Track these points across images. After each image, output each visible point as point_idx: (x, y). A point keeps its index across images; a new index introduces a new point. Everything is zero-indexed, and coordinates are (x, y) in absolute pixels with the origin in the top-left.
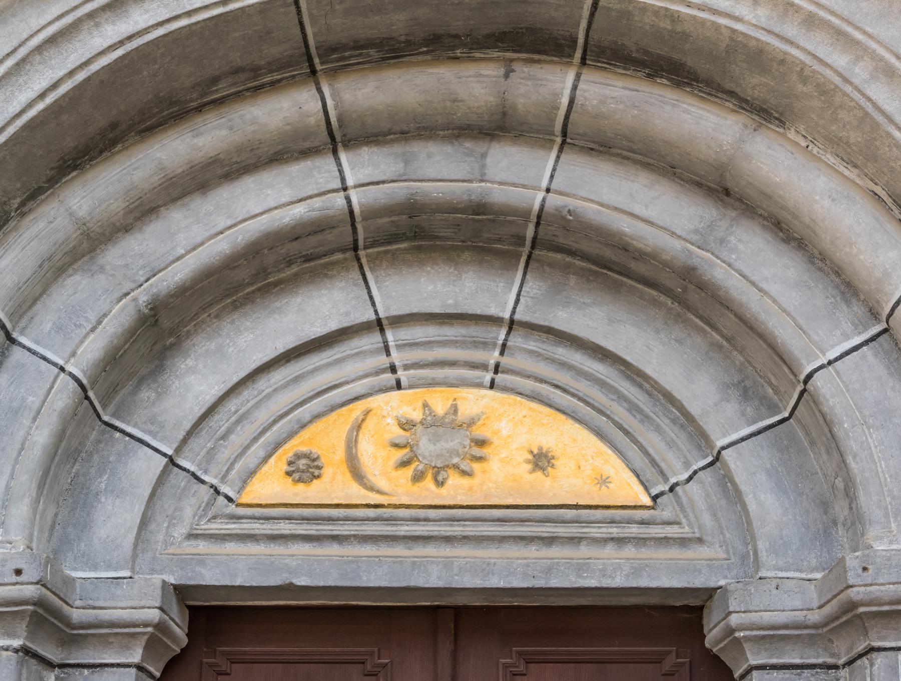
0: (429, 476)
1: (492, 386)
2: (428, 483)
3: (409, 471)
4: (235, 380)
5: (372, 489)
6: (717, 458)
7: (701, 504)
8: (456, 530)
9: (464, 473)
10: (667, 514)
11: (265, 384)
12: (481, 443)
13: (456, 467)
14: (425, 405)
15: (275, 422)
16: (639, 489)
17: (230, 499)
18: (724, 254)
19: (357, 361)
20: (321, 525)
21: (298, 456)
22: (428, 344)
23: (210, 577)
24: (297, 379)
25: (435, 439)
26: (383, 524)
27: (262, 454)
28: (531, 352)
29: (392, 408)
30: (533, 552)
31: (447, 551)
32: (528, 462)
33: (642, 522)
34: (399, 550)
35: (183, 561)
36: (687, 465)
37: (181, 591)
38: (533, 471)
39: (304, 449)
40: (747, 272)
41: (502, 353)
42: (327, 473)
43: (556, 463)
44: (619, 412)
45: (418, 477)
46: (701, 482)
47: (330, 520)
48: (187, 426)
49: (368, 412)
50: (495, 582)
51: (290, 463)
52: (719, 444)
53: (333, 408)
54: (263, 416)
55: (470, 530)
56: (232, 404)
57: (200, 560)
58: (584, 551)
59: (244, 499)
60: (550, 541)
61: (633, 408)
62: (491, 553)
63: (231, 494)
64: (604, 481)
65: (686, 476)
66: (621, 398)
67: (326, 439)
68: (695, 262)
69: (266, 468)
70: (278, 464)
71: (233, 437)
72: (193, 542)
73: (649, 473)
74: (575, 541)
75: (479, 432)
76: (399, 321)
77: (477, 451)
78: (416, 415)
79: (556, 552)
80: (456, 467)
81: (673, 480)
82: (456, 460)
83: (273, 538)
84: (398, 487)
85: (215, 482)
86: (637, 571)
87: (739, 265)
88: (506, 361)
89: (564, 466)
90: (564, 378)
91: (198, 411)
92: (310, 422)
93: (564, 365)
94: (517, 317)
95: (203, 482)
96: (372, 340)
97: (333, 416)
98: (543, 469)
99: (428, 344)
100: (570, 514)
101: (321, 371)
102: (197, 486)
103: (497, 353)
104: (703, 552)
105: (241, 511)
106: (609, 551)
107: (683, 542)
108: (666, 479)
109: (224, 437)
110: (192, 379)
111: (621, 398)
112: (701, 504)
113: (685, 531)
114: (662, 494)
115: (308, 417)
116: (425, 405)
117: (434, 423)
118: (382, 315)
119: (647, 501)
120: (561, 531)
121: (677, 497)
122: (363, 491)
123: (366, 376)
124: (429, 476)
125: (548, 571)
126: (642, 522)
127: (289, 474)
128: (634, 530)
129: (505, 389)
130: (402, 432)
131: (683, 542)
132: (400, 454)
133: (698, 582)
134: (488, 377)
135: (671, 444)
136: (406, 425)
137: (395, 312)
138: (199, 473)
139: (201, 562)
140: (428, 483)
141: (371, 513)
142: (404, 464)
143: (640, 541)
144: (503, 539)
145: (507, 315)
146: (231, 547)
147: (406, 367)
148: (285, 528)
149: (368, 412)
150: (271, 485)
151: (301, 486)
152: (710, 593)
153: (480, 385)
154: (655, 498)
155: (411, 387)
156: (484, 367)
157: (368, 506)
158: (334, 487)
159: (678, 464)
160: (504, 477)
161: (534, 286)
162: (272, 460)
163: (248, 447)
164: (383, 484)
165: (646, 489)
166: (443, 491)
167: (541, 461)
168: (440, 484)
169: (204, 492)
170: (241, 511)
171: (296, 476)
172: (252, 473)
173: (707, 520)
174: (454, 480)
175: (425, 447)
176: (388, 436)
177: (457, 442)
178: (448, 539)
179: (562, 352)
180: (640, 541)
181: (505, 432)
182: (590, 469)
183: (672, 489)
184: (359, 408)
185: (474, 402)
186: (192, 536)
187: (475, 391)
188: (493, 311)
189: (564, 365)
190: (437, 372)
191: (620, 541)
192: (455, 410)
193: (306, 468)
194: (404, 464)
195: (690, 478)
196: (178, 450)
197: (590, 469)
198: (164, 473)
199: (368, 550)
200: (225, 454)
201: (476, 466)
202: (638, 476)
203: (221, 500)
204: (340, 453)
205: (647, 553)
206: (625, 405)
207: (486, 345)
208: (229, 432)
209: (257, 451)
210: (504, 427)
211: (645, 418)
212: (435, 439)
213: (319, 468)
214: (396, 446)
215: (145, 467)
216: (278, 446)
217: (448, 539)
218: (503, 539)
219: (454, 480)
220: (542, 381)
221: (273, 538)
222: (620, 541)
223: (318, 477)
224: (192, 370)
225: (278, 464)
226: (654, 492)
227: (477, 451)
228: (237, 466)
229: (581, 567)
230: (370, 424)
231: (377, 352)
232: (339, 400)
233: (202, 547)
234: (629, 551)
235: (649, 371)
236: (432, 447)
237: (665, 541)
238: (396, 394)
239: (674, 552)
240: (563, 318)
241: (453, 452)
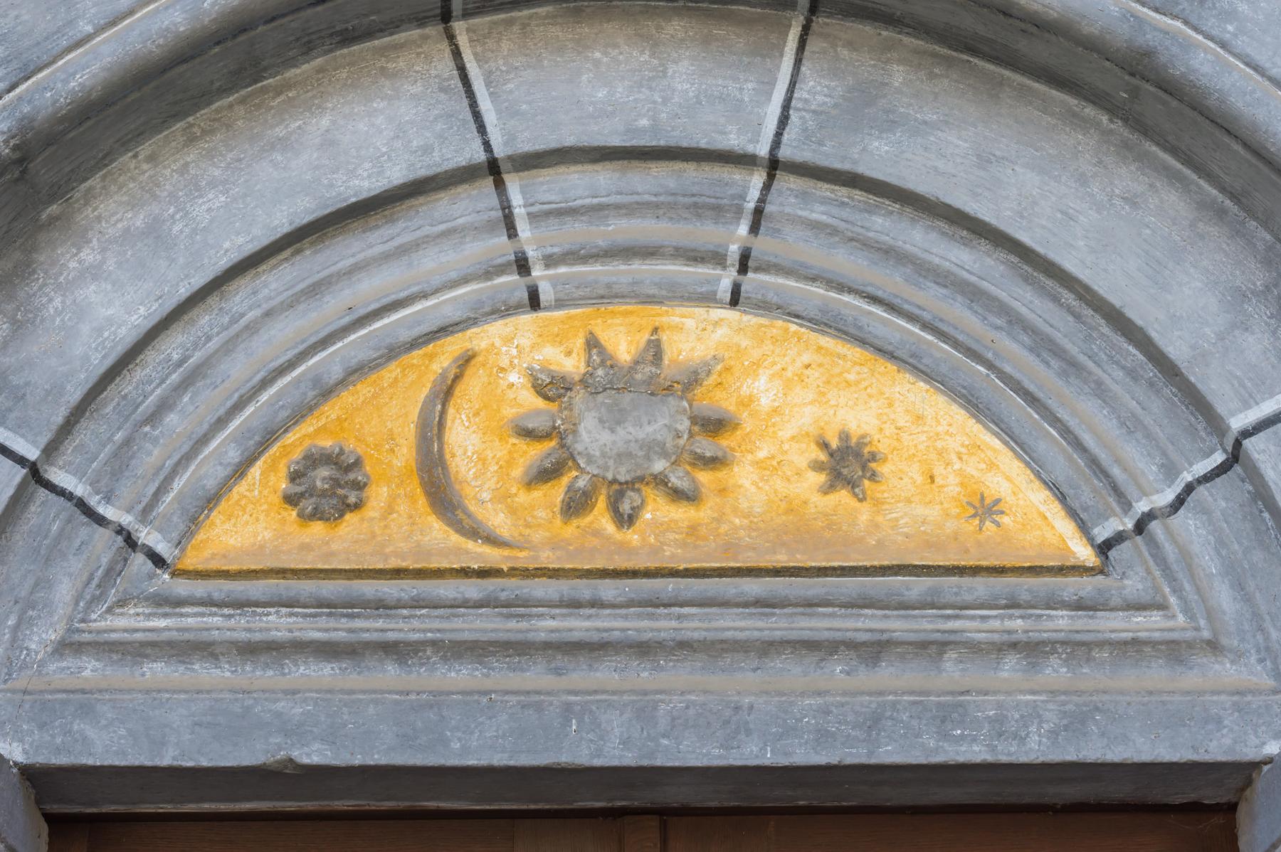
0: (602, 503)
1: (735, 300)
2: (600, 517)
3: (557, 492)
4: (184, 292)
5: (475, 532)
6: (1236, 456)
7: (1208, 563)
8: (663, 626)
9: (678, 495)
10: (1134, 585)
11: (243, 299)
12: (715, 425)
13: (660, 481)
14: (592, 343)
15: (265, 383)
16: (1065, 527)
17: (158, 560)
18: (1210, 24)
19: (444, 250)
20: (359, 617)
21: (314, 460)
22: (597, 211)
23: (104, 744)
24: (315, 290)
25: (614, 419)
26: (499, 611)
27: (234, 455)
28: (816, 226)
29: (518, 351)
30: (837, 671)
31: (642, 675)
32: (817, 466)
33: (1079, 606)
34: (535, 676)
35: (44, 707)
36: (1170, 472)
37: (736, 426)
38: (829, 488)
39: (327, 443)
40: (1262, 58)
41: (755, 229)
42: (378, 496)
43: (884, 469)
44: (1013, 352)
45: (576, 505)
46: (1205, 511)
47: (381, 606)
48: (74, 395)
49: (466, 360)
50: (754, 752)
51: (294, 477)
52: (1237, 423)
53: (393, 352)
54: (238, 370)
55: (695, 625)
56: (173, 345)
57: (84, 702)
58: (952, 671)
59: (192, 561)
60: (874, 650)
61: (1044, 345)
62: (743, 682)
63: (162, 548)
64: (986, 509)
65: (1169, 496)
66: (1015, 322)
67: (379, 421)
68: (1149, 39)
69: (241, 488)
70: (267, 480)
71: (172, 419)
72: (69, 662)
73: (1088, 493)
74: (931, 649)
75: (713, 398)
76: (531, 162)
77: (705, 446)
78: (572, 364)
79: (889, 676)
80: (660, 481)
81: (1142, 507)
82: (659, 466)
83: (251, 650)
84: (513, 511)
85: (126, 519)
86: (1076, 723)
87: (1241, 43)
88: (763, 246)
89: (898, 475)
90: (891, 281)
91: (99, 363)
92: (343, 383)
93: (890, 254)
94: (785, 153)
95: (101, 521)
96: (476, 201)
97: (392, 371)
98: (852, 484)
99: (597, 211)
100: (918, 586)
101: (367, 269)
102: (86, 530)
103: (743, 229)
104: (1226, 672)
105: (183, 588)
106: (1010, 669)
107: (1174, 651)
108: (1127, 506)
109: (154, 418)
110: (90, 292)
111: (1015, 322)
112: (1208, 563)
113: (1170, 623)
114: (1119, 538)
115: (336, 372)
116: (592, 343)
117: (610, 382)
118: (499, 151)
119: (1084, 553)
120: (897, 625)
121: (1153, 543)
122: (455, 538)
123: (465, 280)
124: (602, 503)
125: (874, 722)
126: (1079, 606)
127: (291, 500)
128: (1062, 621)
129: (765, 307)
130: (540, 403)
131: (1174, 651)
132: (535, 452)
133: (1217, 748)
134: (726, 280)
135: (1132, 426)
136: (552, 387)
137: (526, 145)
138: (93, 501)
139: (86, 710)
140: (600, 517)
141: (472, 589)
142: (545, 474)
143: (1078, 649)
144: (768, 648)
145: (763, 150)
146: (156, 671)
147: (550, 261)
148: (278, 625)
149: (466, 360)
150: (251, 526)
151: (318, 528)
152: (1244, 773)
153: (708, 299)
154: (1104, 548)
155: (560, 304)
156: (718, 258)
157: (465, 573)
158: (391, 523)
159: (1149, 470)
160: (765, 491)
161: (817, 88)
162: (256, 471)
163: (204, 440)
164: (498, 521)
165: (1084, 528)
166: (632, 536)
167: (847, 463)
168: (626, 520)
169: (103, 544)
170: (183, 588)
171: (308, 505)
172: (212, 500)
173: (1224, 598)
174: (657, 509)
175: (593, 436)
176: (509, 412)
177: (662, 423)
178: (644, 649)
179: (885, 224)
180: (1078, 649)
181: (765, 402)
182: (954, 475)
183: (1140, 527)
184: (446, 353)
185: (697, 334)
186: (68, 646)
187: (700, 312)
188: (733, 141)
189: (890, 254)
190: (620, 266)
191: (1033, 650)
192: (655, 351)
193: (329, 487)
194: (545, 474)
195: (1179, 502)
196: (51, 450)
197: (954, 475)
198: (22, 487)
199: (461, 676)
200: (152, 456)
201: (704, 477)
202: (1062, 498)
203: (139, 561)
204: (405, 454)
205: (1092, 677)
206: (1021, 334)
207: (720, 211)
208: (164, 406)
209: (224, 448)
210: (762, 389)
211: (1072, 367)
212: (614, 419)
213: (359, 486)
214: (528, 434)
215: (43, 552)
216: (269, 437)
217: (644, 649)
218: (768, 648)
219: (657, 509)
220: (842, 288)
221: (251, 650)
222: (1033, 650)
223: (357, 506)
224: (93, 273)
225: (267, 480)
226: (1103, 532)
227: (705, 446)
228: (178, 484)
229: (949, 714)
230: (472, 386)
231: (490, 227)
232: (405, 335)
233: (90, 669)
234: (1055, 672)
235: (1070, 264)
236: (606, 437)
237: (1132, 648)
238: (527, 319)
239: (1156, 675)
240: (878, 155)
241: (653, 448)
